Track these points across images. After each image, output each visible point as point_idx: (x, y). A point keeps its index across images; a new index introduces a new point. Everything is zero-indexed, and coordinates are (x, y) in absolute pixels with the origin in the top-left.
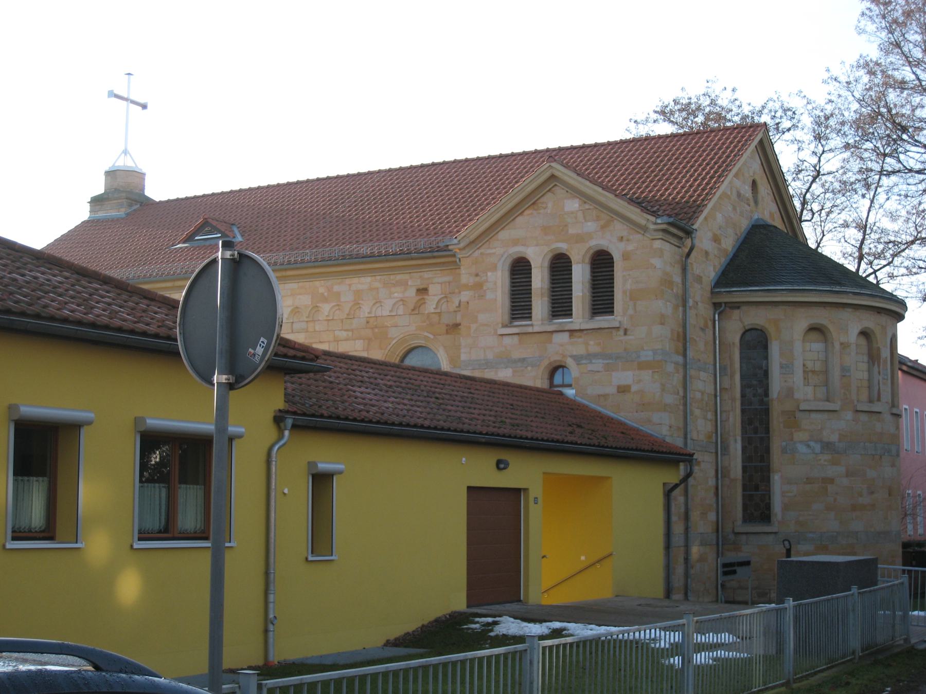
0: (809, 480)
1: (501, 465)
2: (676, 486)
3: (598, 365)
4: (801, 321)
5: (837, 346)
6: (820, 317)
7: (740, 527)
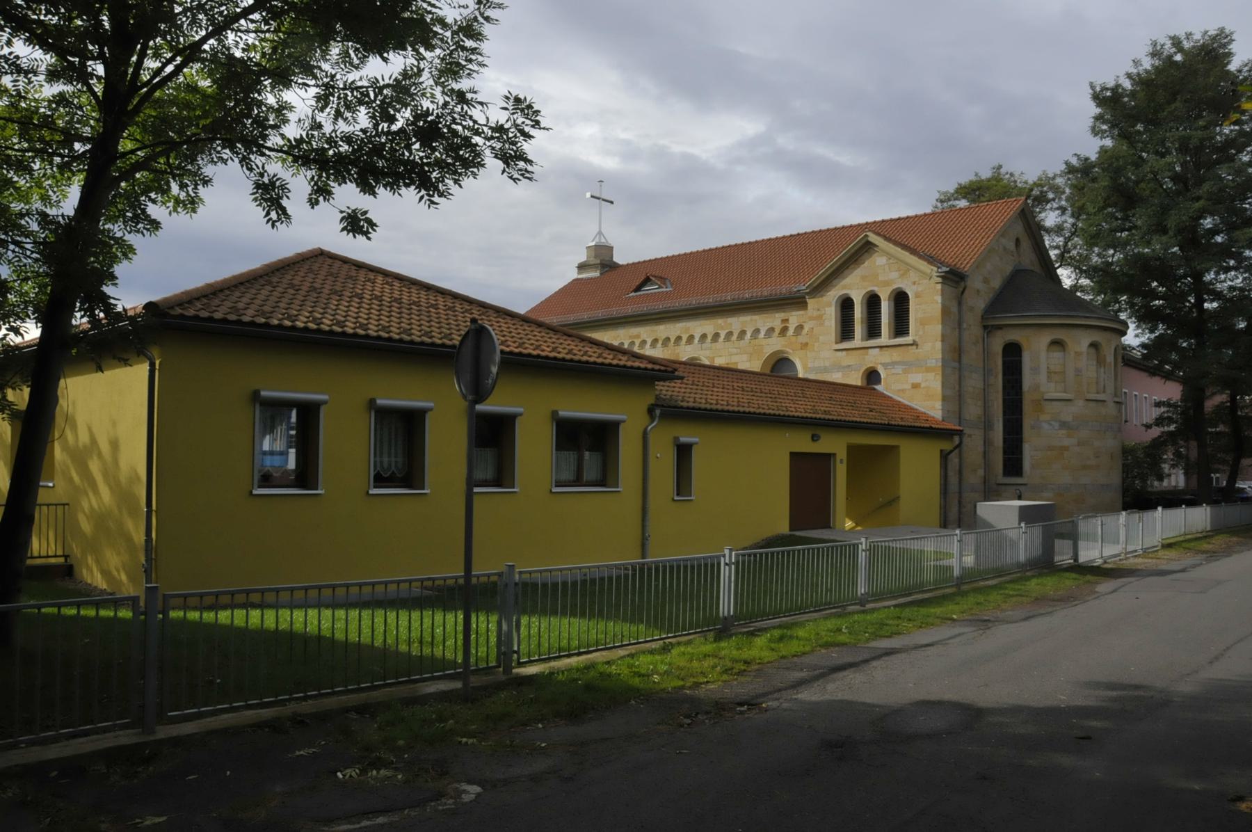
0: (1050, 448)
1: (815, 438)
2: (951, 452)
3: (899, 369)
4: (1045, 338)
7: (1001, 479)
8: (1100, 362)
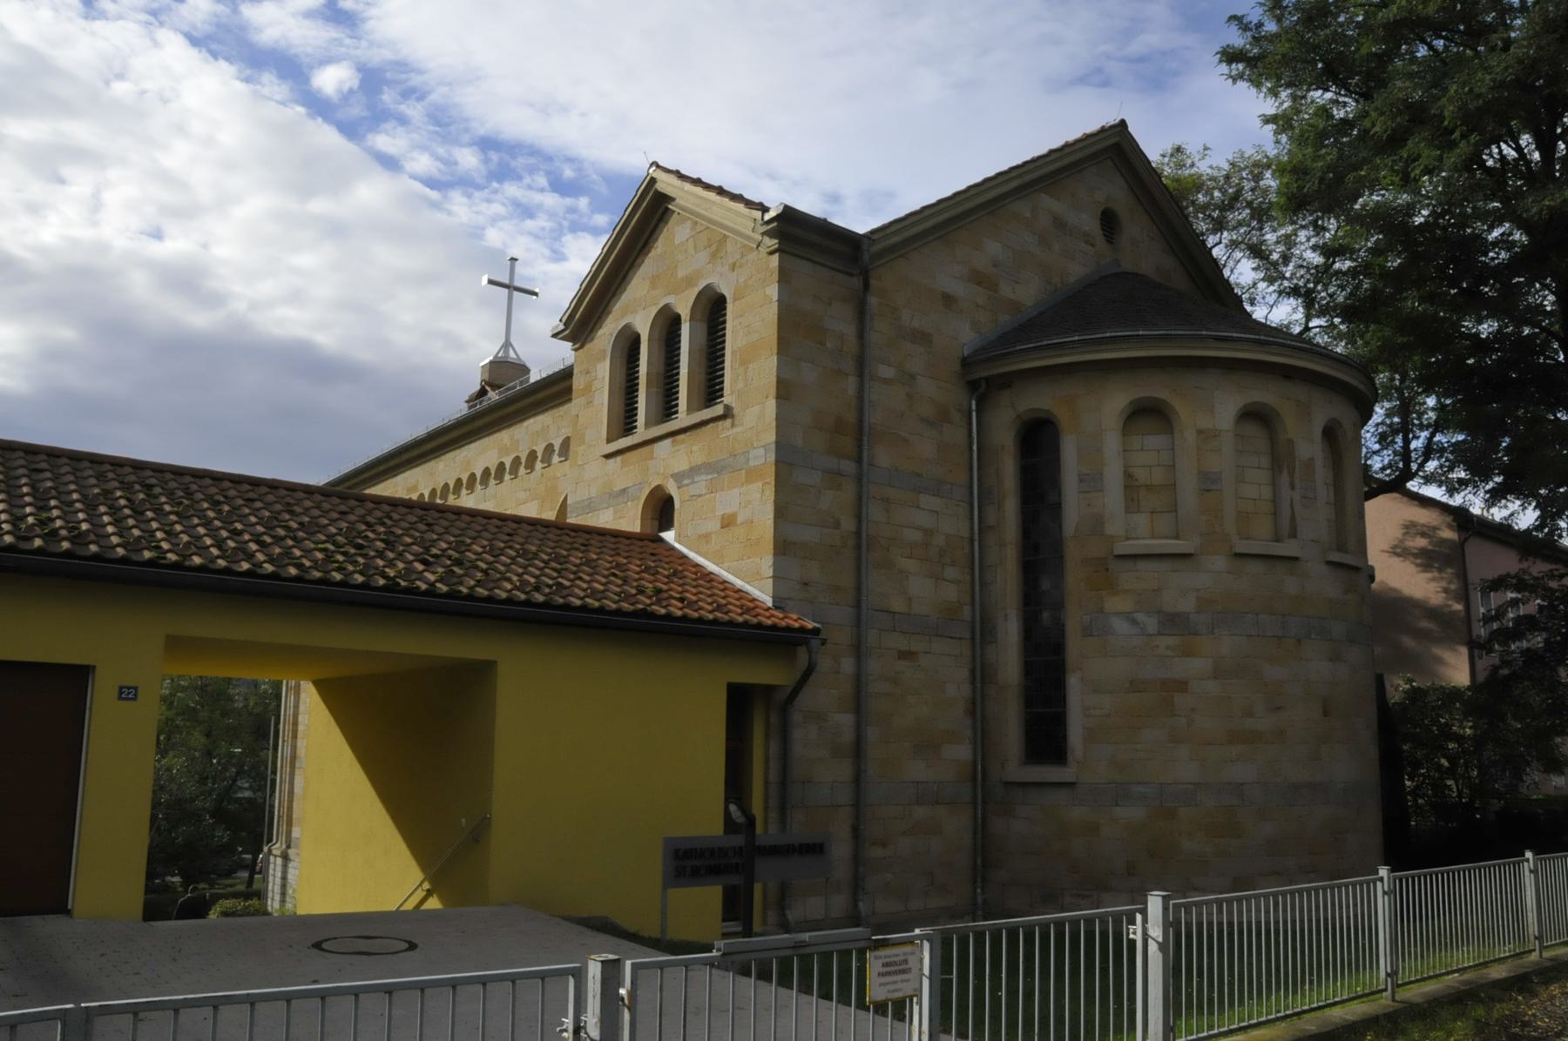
4: (1115, 401)
5: (1190, 436)
6: (1155, 388)
8: (1280, 459)
